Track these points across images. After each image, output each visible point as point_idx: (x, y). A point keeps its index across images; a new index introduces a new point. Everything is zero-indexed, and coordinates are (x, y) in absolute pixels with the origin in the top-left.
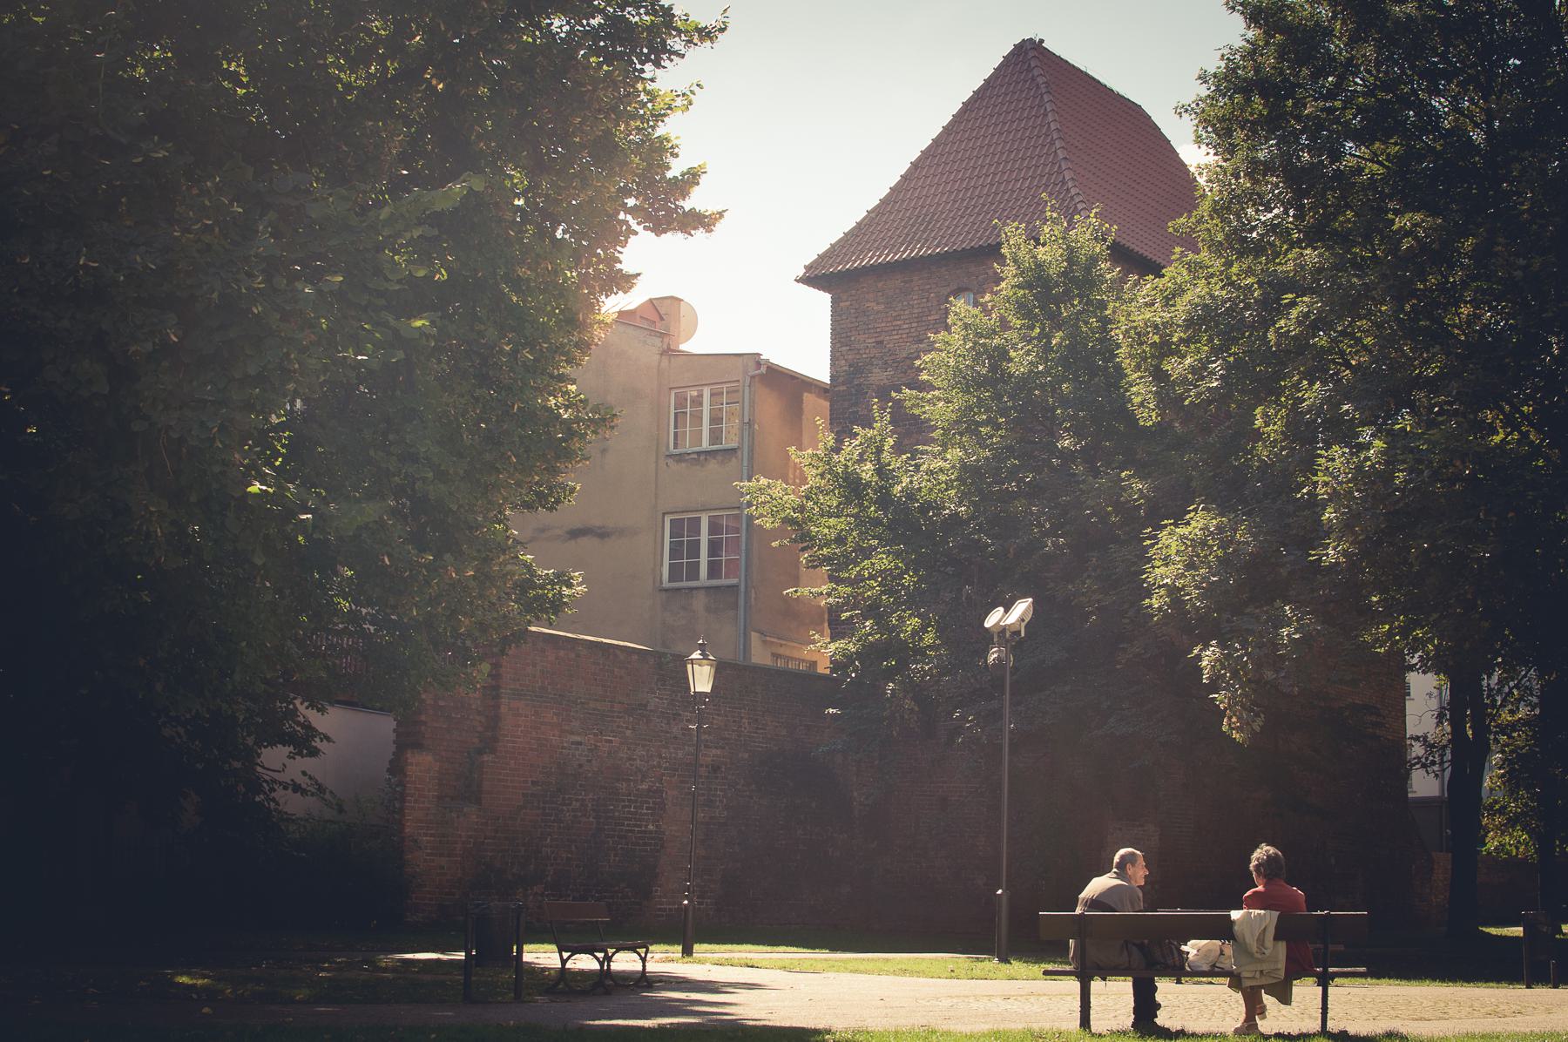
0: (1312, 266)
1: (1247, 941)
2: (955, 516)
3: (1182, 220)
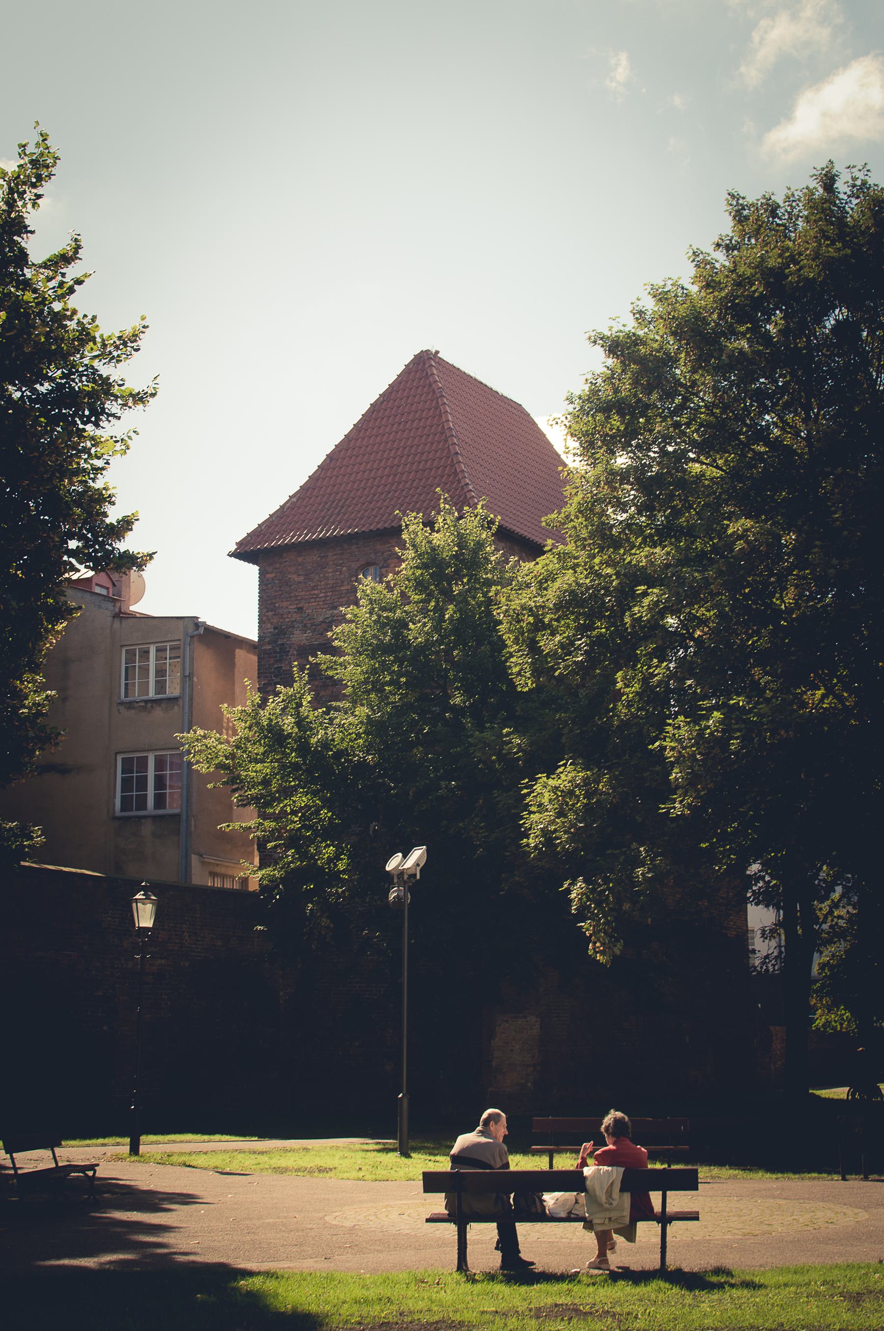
0: (661, 563)
1: (597, 1193)
2: (363, 764)
3: (554, 516)
